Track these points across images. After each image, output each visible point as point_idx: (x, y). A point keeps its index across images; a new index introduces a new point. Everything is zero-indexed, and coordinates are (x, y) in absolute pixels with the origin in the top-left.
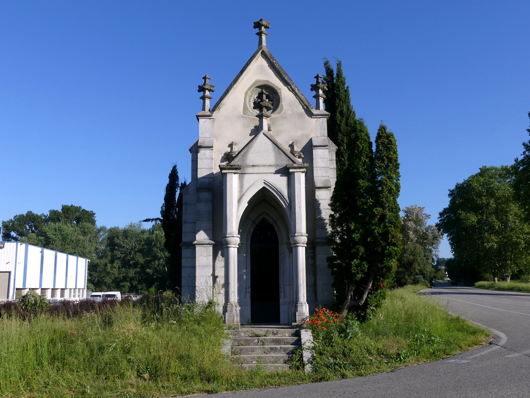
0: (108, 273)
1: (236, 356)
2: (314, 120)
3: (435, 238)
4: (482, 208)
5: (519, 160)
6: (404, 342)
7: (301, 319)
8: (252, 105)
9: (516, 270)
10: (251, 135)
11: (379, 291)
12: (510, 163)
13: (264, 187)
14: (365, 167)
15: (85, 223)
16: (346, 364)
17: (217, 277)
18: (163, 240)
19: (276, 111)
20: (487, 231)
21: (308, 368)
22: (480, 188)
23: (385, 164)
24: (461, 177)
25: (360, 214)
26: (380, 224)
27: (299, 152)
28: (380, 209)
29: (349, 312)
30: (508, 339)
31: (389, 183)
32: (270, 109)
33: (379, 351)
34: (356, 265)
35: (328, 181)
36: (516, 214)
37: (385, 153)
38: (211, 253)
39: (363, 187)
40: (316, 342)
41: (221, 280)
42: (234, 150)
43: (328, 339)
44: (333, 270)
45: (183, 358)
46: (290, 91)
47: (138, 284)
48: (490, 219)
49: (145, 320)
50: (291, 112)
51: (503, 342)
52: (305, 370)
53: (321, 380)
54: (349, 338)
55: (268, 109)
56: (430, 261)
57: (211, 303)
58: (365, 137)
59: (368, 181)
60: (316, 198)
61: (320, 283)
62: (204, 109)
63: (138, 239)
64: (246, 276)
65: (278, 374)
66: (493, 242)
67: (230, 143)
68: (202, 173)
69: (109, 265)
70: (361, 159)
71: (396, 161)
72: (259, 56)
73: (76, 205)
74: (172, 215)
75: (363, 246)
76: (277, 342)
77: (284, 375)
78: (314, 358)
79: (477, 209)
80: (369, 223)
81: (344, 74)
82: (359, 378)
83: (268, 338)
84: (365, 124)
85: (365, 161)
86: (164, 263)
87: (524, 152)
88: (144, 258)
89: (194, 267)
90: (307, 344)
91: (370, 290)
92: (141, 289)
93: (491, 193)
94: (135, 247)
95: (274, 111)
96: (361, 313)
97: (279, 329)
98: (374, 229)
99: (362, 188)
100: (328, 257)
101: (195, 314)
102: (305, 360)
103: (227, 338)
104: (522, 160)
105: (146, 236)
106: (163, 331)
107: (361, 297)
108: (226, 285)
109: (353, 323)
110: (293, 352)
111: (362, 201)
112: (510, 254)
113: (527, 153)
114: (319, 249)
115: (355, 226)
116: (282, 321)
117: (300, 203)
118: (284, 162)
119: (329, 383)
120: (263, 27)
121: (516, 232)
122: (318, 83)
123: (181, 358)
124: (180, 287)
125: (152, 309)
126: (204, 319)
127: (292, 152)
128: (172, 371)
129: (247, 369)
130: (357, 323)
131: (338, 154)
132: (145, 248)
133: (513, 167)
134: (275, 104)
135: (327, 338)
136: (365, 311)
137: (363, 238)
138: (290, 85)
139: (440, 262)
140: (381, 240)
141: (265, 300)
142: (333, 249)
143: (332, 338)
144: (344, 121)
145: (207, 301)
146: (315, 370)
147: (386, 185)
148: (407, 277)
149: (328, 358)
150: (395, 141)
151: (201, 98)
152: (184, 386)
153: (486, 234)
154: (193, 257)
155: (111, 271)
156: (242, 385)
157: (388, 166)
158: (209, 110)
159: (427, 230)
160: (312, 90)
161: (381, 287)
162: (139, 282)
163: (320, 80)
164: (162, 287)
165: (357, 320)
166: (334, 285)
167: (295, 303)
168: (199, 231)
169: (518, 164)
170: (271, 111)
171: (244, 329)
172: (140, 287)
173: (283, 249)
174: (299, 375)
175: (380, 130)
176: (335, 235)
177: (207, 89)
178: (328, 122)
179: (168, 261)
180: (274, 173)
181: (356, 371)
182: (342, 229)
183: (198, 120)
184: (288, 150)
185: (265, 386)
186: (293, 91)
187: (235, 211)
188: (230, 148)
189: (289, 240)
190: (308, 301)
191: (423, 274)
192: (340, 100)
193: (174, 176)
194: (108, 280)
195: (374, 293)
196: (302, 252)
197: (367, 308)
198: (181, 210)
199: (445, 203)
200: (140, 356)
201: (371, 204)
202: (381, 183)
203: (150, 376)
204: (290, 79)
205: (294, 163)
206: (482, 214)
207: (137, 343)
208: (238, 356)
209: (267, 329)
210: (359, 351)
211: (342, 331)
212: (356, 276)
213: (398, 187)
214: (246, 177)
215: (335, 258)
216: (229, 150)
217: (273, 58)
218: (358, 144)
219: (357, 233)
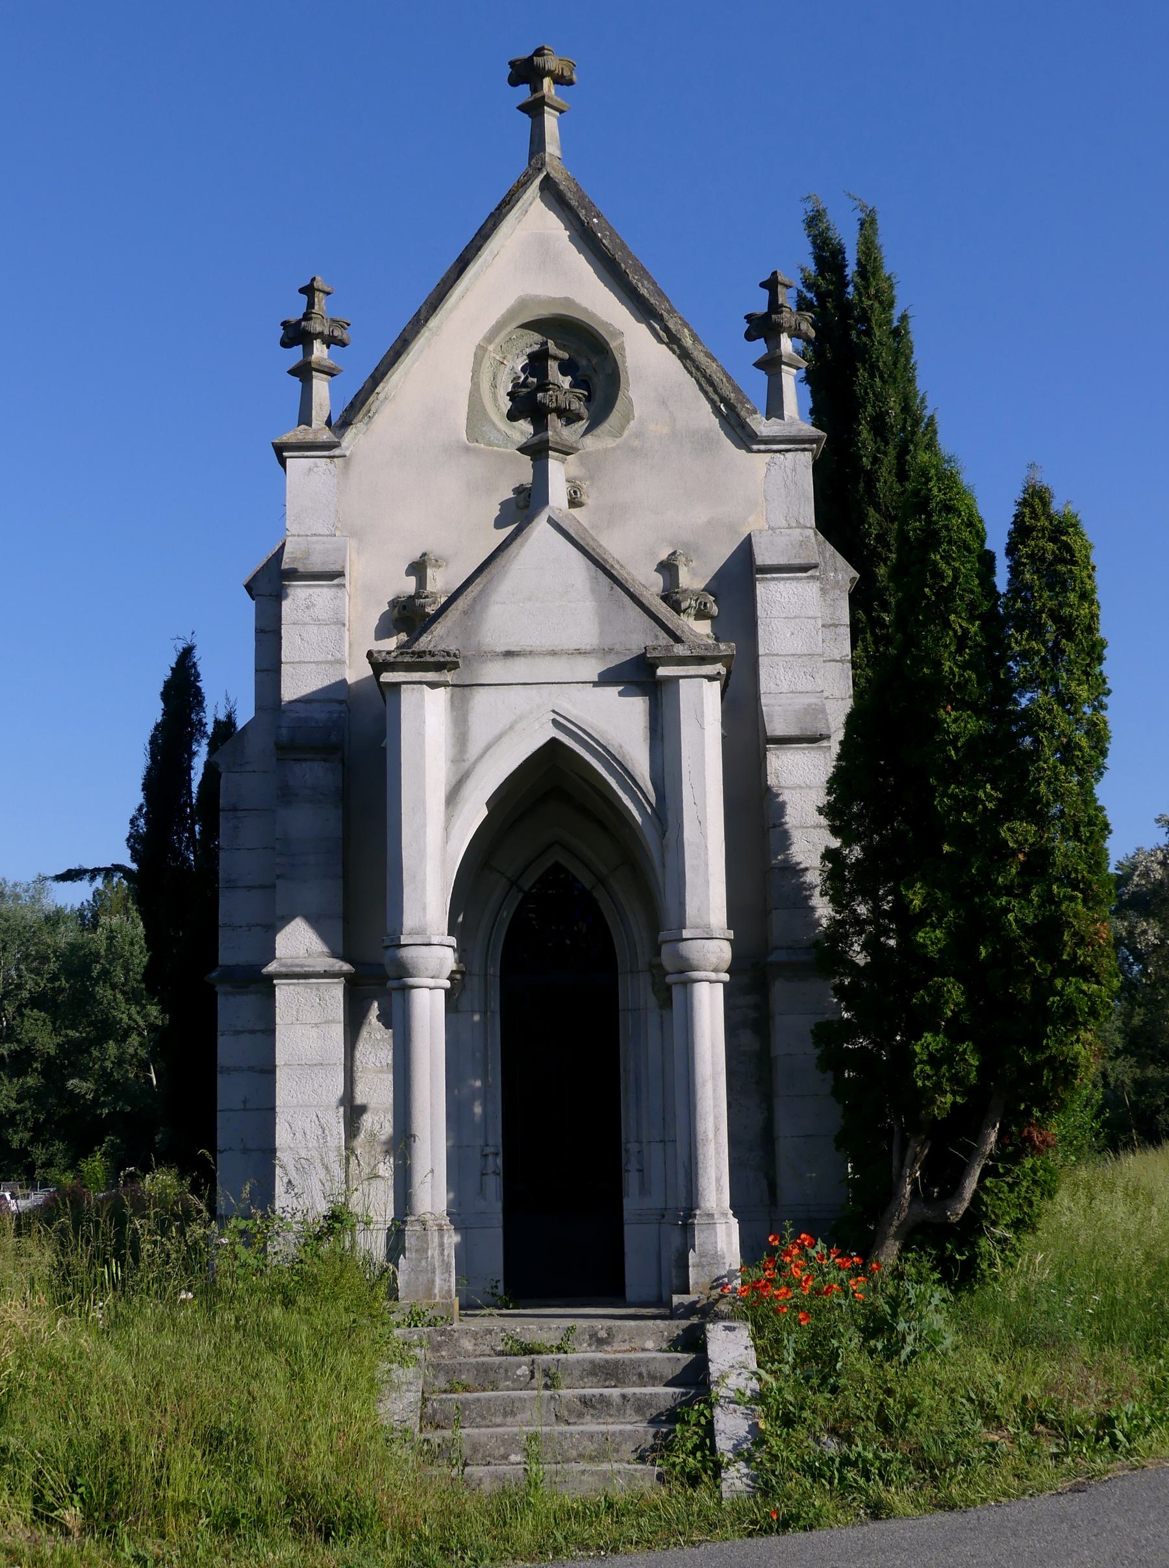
1: (440, 1432)
2: (759, 462)
6: (1134, 1372)
7: (707, 1280)
8: (506, 404)
10: (499, 523)
11: (1028, 1163)
13: (553, 741)
16: (888, 1462)
17: (363, 1109)
18: (141, 959)
19: (605, 426)
21: (735, 1479)
23: (1044, 643)
26: (1027, 890)
27: (697, 595)
28: (1026, 829)
29: (905, 1248)
31: (1063, 722)
32: (579, 418)
33: (1030, 1406)
34: (930, 1055)
35: (818, 711)
37: (1045, 599)
38: (337, 1009)
39: (957, 736)
40: (772, 1372)
41: (379, 1122)
42: (430, 587)
43: (819, 1361)
44: (839, 1076)
45: (220, 1440)
46: (661, 341)
47: (32, 1142)
49: (66, 1291)
50: (666, 430)
52: (724, 1486)
53: (785, 1524)
55: (570, 417)
57: (337, 1220)
58: (966, 535)
59: (978, 712)
60: (771, 780)
61: (785, 1128)
62: (305, 418)
63: (33, 950)
64: (484, 1107)
65: (610, 1506)
67: (416, 556)
68: (296, 684)
70: (947, 625)
71: (1090, 629)
74: (177, 854)
75: (960, 978)
77: (637, 1508)
78: (758, 1438)
81: (889, 267)
82: (941, 1517)
83: (571, 1357)
84: (966, 479)
85: (965, 631)
86: (143, 1053)
88: (56, 1031)
89: (268, 1071)
90: (734, 1381)
91: (991, 1157)
92: (43, 1165)
94: (19, 987)
95: (595, 422)
97: (618, 1323)
98: (1006, 910)
99: (953, 743)
100: (819, 1026)
101: (272, 1261)
102: (723, 1444)
103: (403, 1363)
105: (66, 936)
106: (140, 1331)
107: (953, 1190)
108: (402, 1142)
109: (921, 1297)
110: (673, 1416)
111: (953, 797)
114: (780, 990)
116: (630, 1293)
117: (701, 804)
118: (637, 637)
119: (815, 1535)
120: (547, 81)
122: (775, 306)
123: (213, 1441)
124: (214, 1153)
125: (97, 1247)
126: (309, 1283)
127: (671, 597)
128: (176, 1493)
129: (487, 1486)
130: (939, 1294)
131: (862, 598)
132: (61, 990)
134: (599, 395)
135: (817, 1357)
136: (974, 1245)
137: (962, 943)
138: (660, 319)
140: (1033, 952)
141: (561, 1205)
142: (840, 990)
143: (835, 1355)
144: (889, 461)
145: (323, 1208)
146: (764, 1488)
147: (1051, 729)
149: (817, 1440)
150: (1087, 547)
151: (292, 372)
152: (226, 1556)
156: (464, 1549)
157: (1056, 651)
158: (328, 423)
160: (749, 336)
161: (1034, 1147)
162: (38, 1134)
163: (786, 298)
164: (135, 1156)
165: (939, 1282)
166: (842, 1141)
167: (684, 1213)
168: (286, 920)
170: (582, 425)
171: (475, 1324)
172: (39, 1154)
173: (634, 992)
174: (695, 1508)
175: (1024, 503)
176: (846, 936)
177: (319, 335)
178: (818, 468)
179: (163, 1042)
180: (596, 684)
181: (929, 1490)
182: (876, 911)
183: (283, 462)
184: (651, 584)
185: (557, 1551)
186: (672, 341)
187: (435, 839)
189: (658, 952)
190: (738, 1207)
192: (873, 369)
193: (182, 689)
195: (1008, 1172)
196: (709, 1006)
197: (980, 1232)
198: (212, 830)
200: (44, 1434)
201: (990, 806)
202: (1031, 721)
203: (88, 1516)
204: (660, 294)
205: (678, 640)
207: (32, 1383)
208: (448, 1433)
209: (569, 1323)
210: (945, 1407)
211: (876, 1327)
212: (933, 1102)
213: (1098, 737)
214: (481, 700)
215: (847, 1030)
216: (409, 585)
217: (590, 207)
218: (935, 563)
219: (934, 927)
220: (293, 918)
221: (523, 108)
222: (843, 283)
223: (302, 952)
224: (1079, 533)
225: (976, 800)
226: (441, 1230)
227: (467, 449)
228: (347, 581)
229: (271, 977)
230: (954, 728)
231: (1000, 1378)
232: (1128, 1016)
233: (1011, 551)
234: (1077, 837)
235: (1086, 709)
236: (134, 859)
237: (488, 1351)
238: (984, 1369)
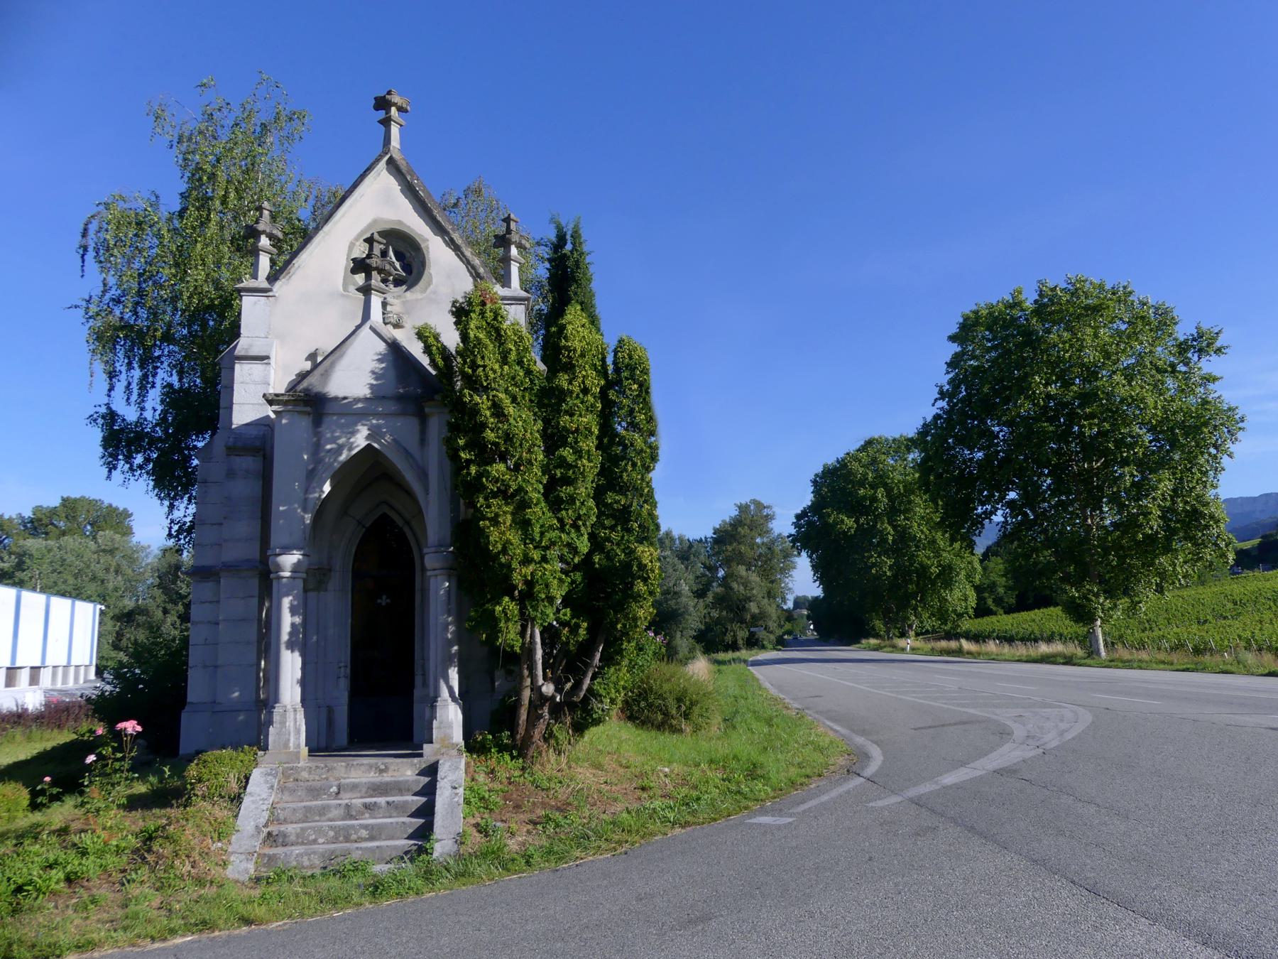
3: (787, 556)
12: (910, 429)
19: (417, 287)
24: (830, 457)
51: (870, 770)
67: (312, 350)
93: (881, 480)
120: (393, 109)
122: (509, 231)
134: (415, 271)
139: (798, 603)
170: (404, 287)
177: (264, 232)
199: (806, 498)
221: (381, 122)
226: (295, 710)
228: (272, 361)
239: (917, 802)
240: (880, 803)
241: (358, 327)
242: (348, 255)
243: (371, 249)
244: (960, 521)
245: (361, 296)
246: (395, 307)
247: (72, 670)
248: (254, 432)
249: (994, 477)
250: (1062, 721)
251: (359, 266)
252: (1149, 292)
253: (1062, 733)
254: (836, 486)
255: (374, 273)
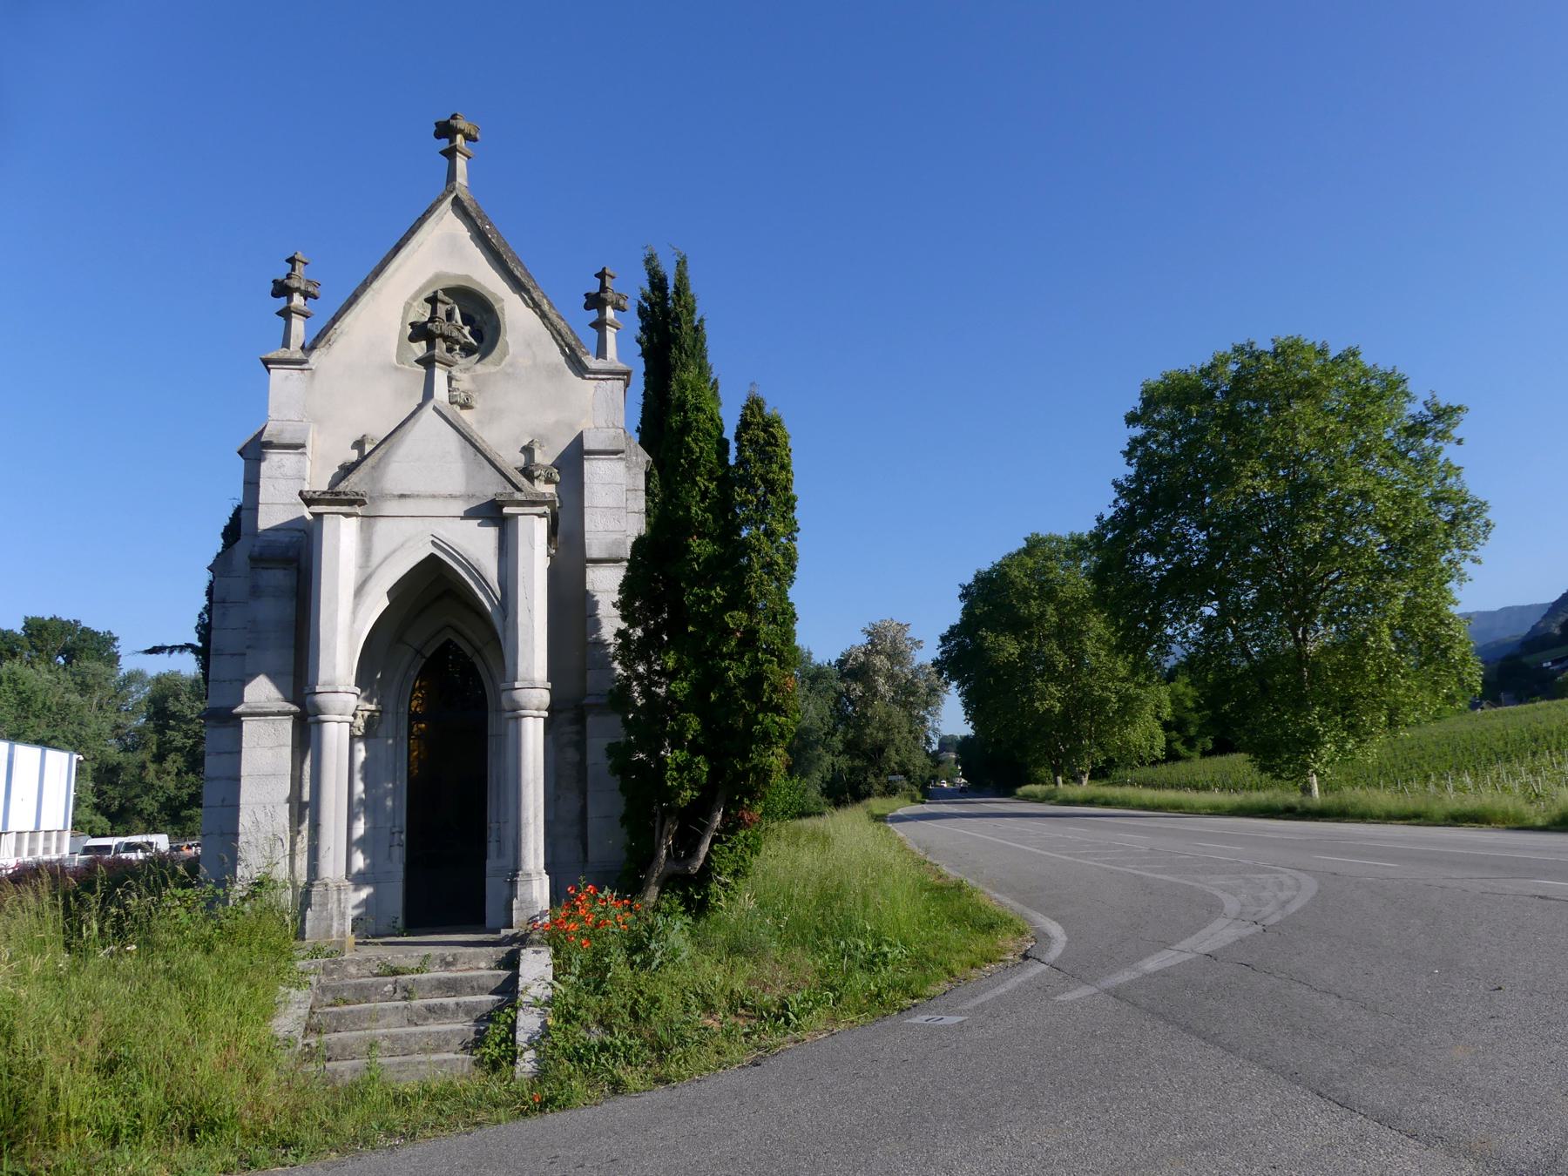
0: (148, 788)
2: (589, 386)
3: (933, 691)
4: (1029, 625)
5: (1106, 518)
6: (809, 963)
7: (525, 919)
9: (1100, 758)
12: (1085, 526)
13: (432, 556)
14: (715, 508)
15: (86, 663)
19: (490, 358)
20: (1041, 675)
21: (526, 1064)
22: (1026, 581)
24: (986, 561)
25: (690, 629)
29: (662, 891)
30: (1068, 943)
31: (766, 546)
36: (1099, 638)
39: (699, 556)
43: (596, 976)
48: (1045, 649)
51: (1054, 953)
54: (654, 966)
56: (923, 742)
58: (708, 425)
59: (714, 541)
62: (286, 344)
66: (1052, 698)
67: (359, 437)
69: (152, 767)
70: (695, 483)
71: (786, 489)
72: (446, 211)
73: (66, 615)
75: (698, 714)
76: (451, 987)
78: (546, 1030)
79: (1019, 626)
80: (714, 652)
83: (425, 976)
85: (707, 488)
87: (1116, 501)
93: (1048, 593)
96: (694, 894)
98: (728, 669)
99: (696, 560)
102: (521, 1037)
104: (1113, 518)
107: (692, 852)
110: (489, 1018)
111: (696, 595)
112: (1087, 724)
113: (1122, 503)
115: (679, 661)
116: (488, 924)
117: (530, 598)
118: (491, 487)
120: (459, 137)
121: (1100, 678)
122: (603, 288)
133: (1093, 536)
134: (487, 338)
136: (707, 887)
138: (528, 292)
139: (945, 743)
140: (744, 696)
141: (440, 867)
143: (608, 968)
147: (759, 552)
148: (871, 779)
153: (1039, 683)
154: (235, 751)
155: (156, 782)
158: (303, 348)
159: (915, 673)
160: (587, 307)
165: (684, 913)
168: (253, 676)
169: (1104, 527)
170: (477, 356)
175: (747, 407)
177: (297, 290)
180: (462, 518)
182: (650, 670)
186: (536, 306)
188: (356, 452)
190: (549, 867)
191: (906, 773)
192: (681, 348)
194: (148, 804)
195: (729, 840)
196: (533, 734)
199: (952, 613)
204: (529, 276)
205: (519, 490)
206: (1029, 638)
211: (636, 947)
213: (790, 559)
214: (382, 526)
215: (630, 748)
217: (484, 218)
219: (682, 680)
220: (257, 675)
222: (665, 297)
223: (263, 698)
224: (781, 427)
225: (711, 597)
226: (339, 888)
227: (397, 369)
228: (309, 450)
229: (240, 715)
230: (697, 550)
231: (717, 978)
232: (846, 733)
233: (738, 438)
234: (775, 621)
235: (783, 540)
236: (200, 640)
237: (366, 972)
238: (713, 974)
239: (1116, 994)
240: (1068, 997)
241: (420, 407)
242: (404, 319)
243: (434, 311)
244: (1136, 640)
245: (422, 370)
246: (464, 382)
247: (41, 836)
248: (285, 538)
249: (1186, 585)
250: (1281, 890)
251: (420, 332)
252: (1376, 357)
253: (1284, 905)
254: (991, 600)
255: (439, 341)
